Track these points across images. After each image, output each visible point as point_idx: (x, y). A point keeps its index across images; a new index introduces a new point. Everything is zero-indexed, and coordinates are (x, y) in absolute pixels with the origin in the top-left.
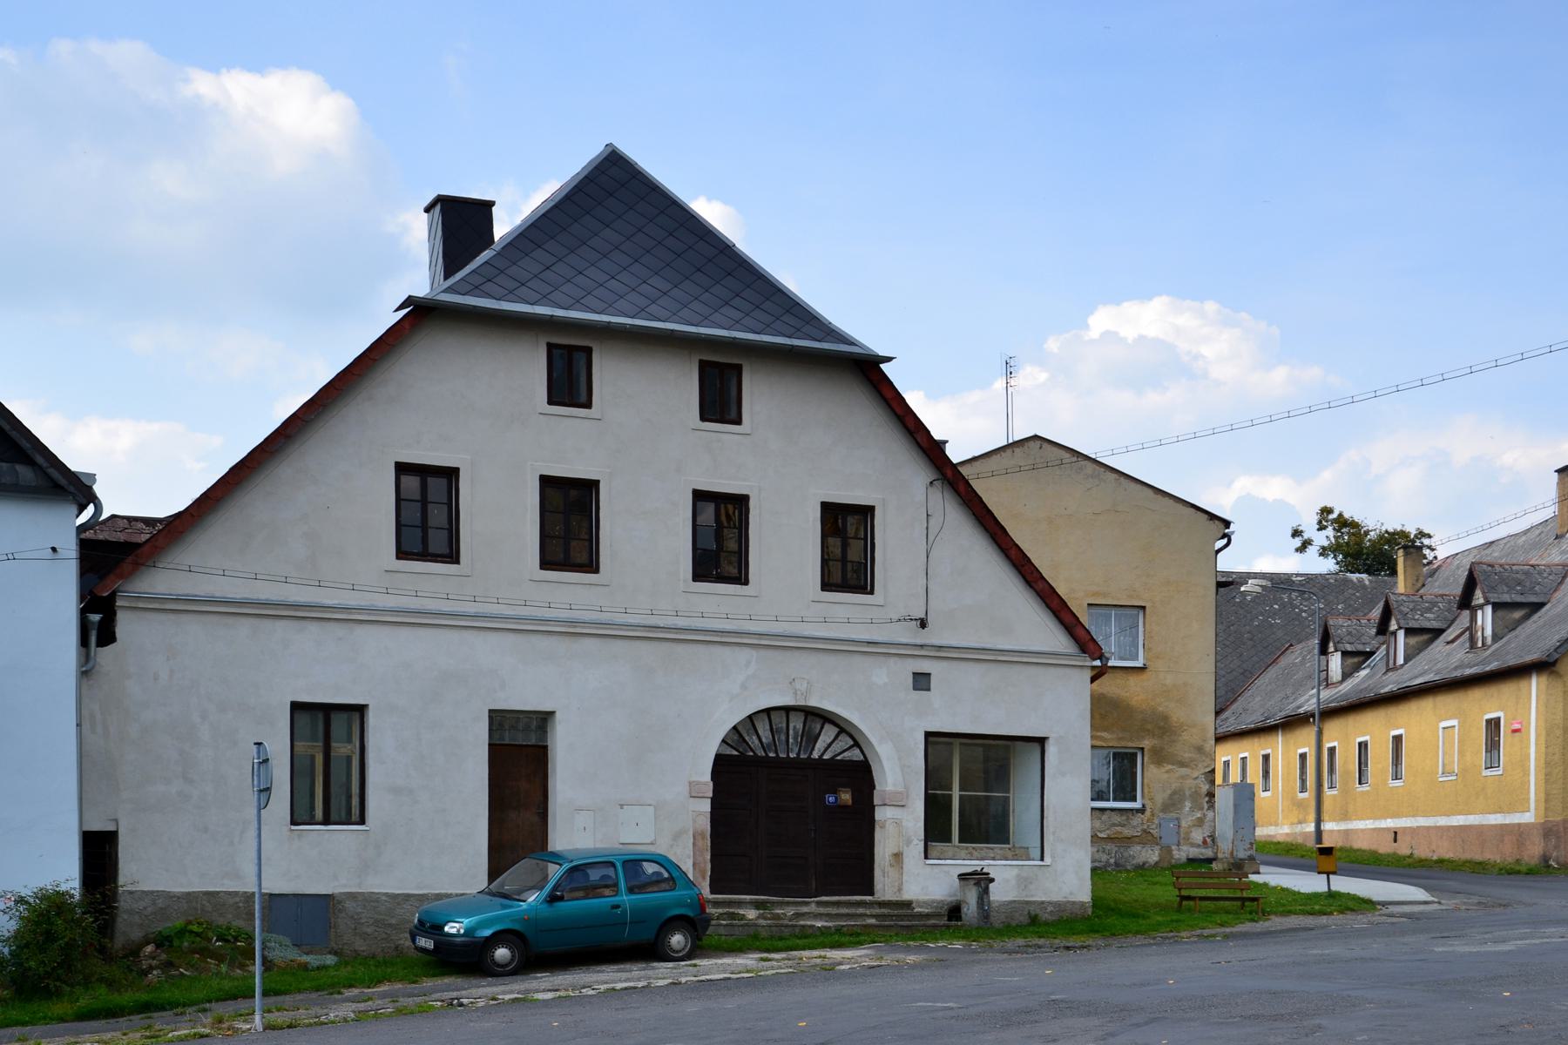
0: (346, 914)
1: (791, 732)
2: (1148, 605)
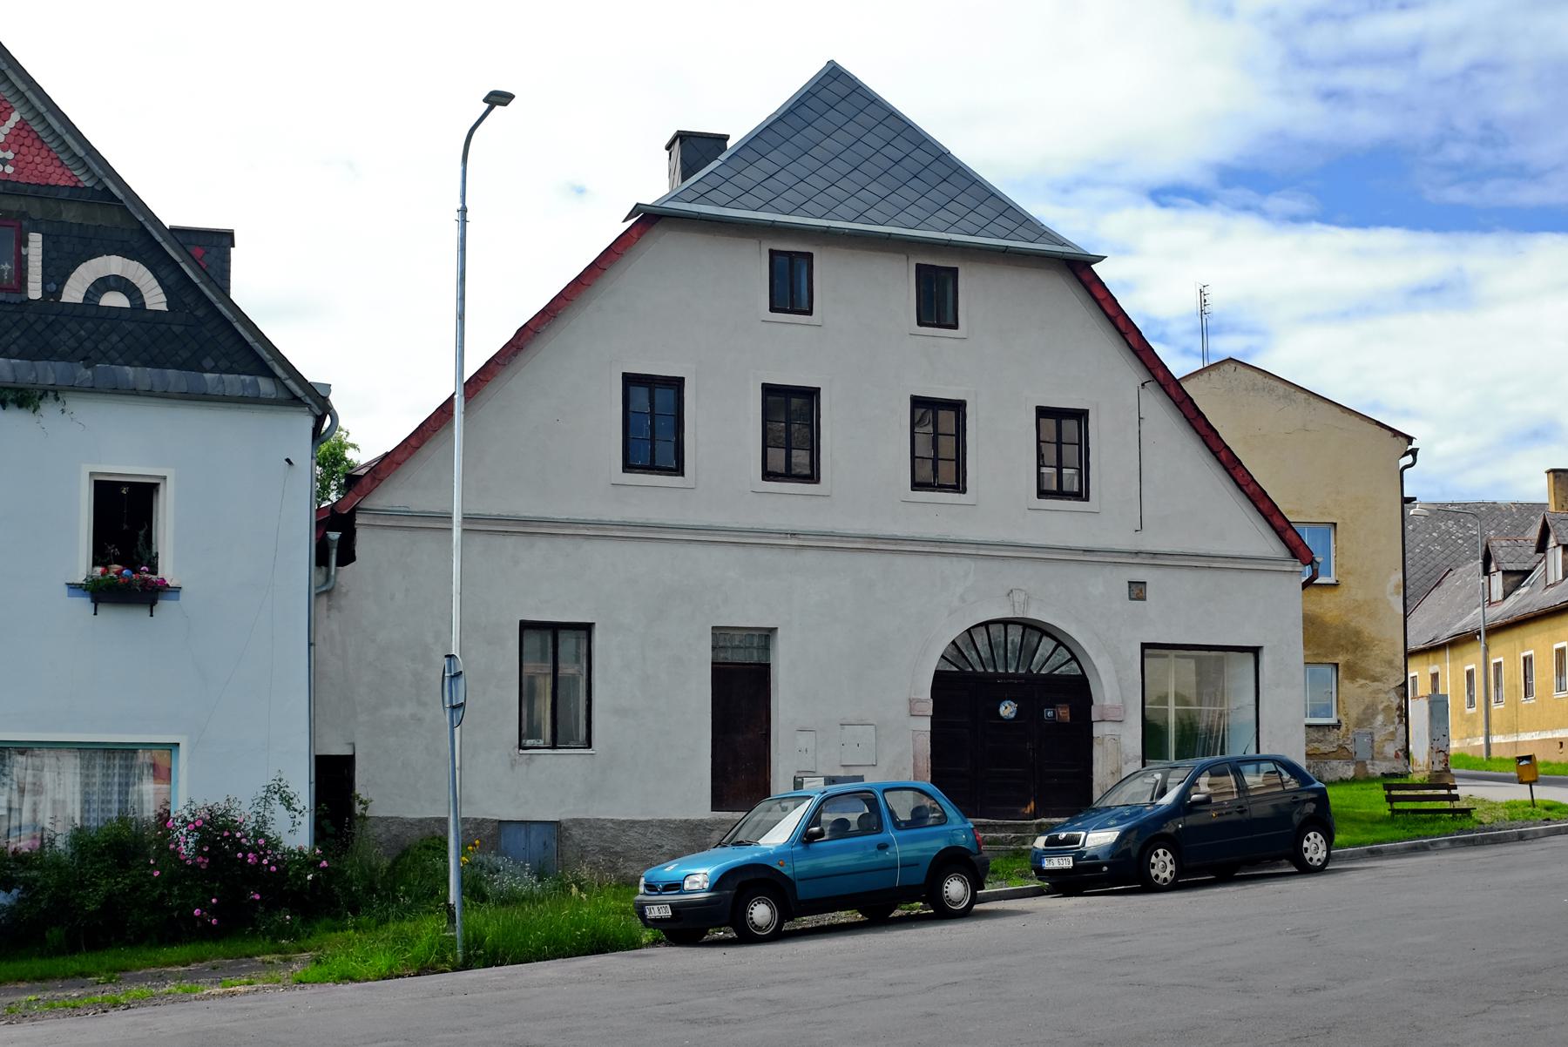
1: (1009, 646)
2: (1338, 522)
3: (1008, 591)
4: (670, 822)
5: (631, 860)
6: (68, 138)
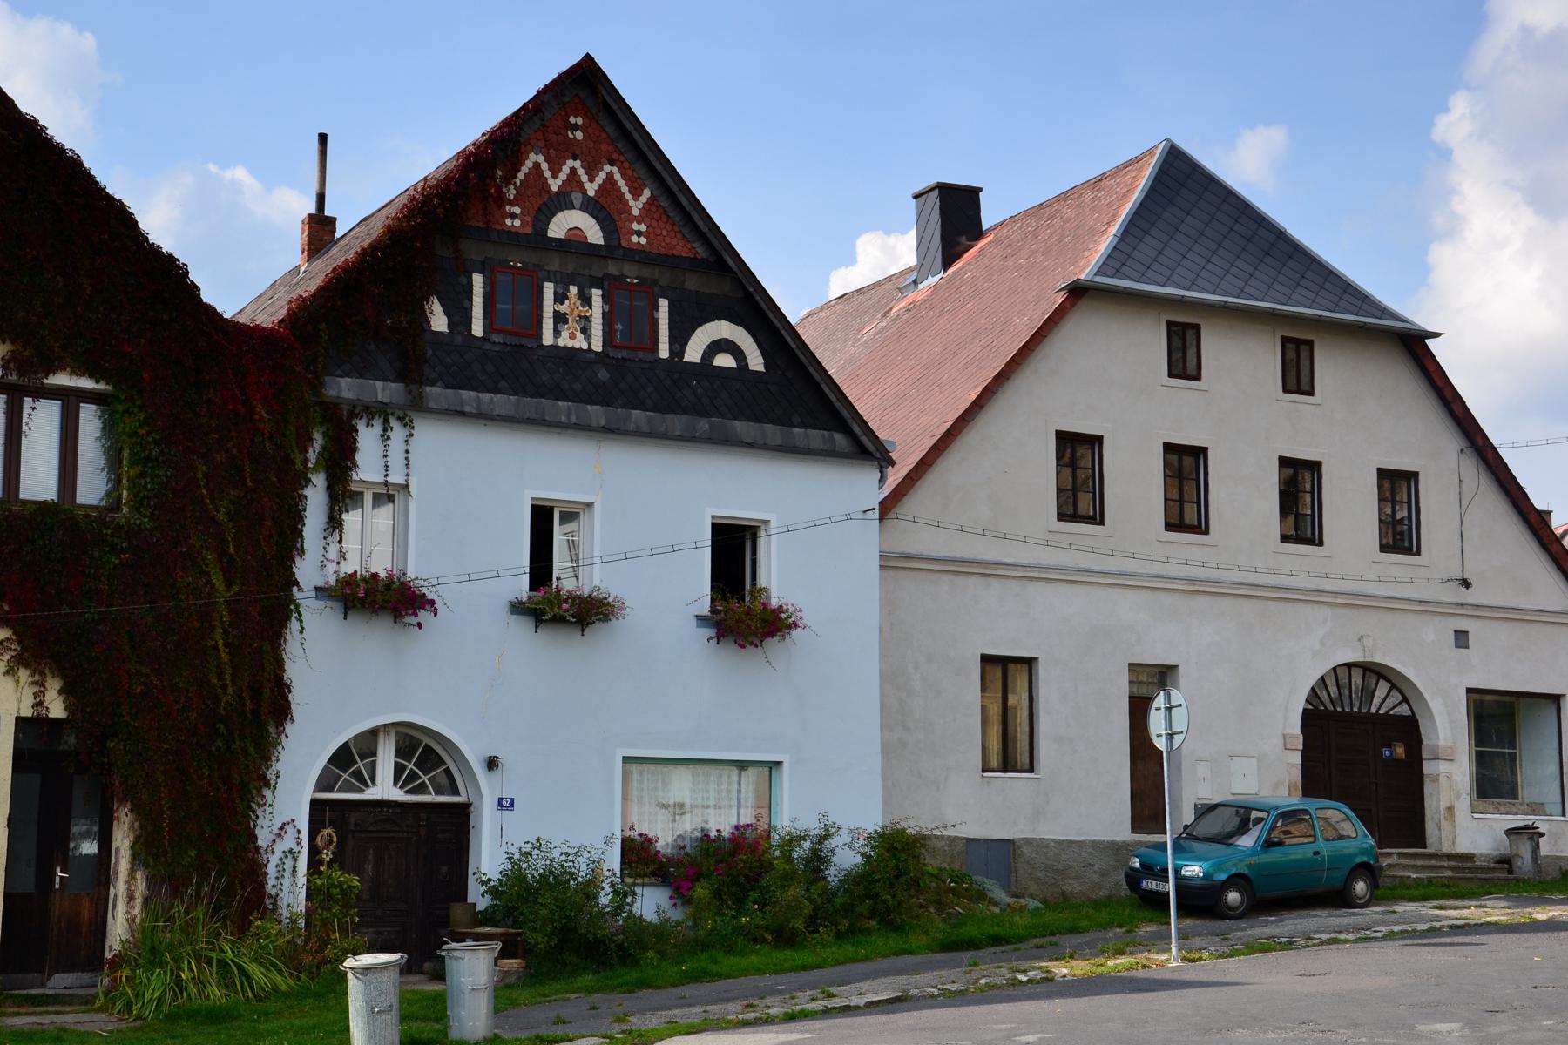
1: (1353, 687)
3: (1359, 636)
4: (1101, 842)
5: (1069, 878)
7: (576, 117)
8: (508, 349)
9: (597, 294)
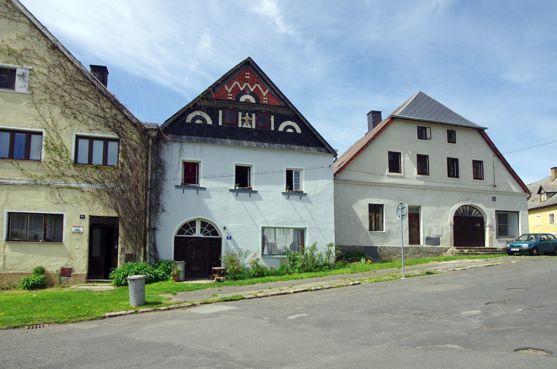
0: (245, 259)
1: (467, 211)
6: (280, 95)
7: (247, 73)
8: (229, 128)
9: (254, 115)
